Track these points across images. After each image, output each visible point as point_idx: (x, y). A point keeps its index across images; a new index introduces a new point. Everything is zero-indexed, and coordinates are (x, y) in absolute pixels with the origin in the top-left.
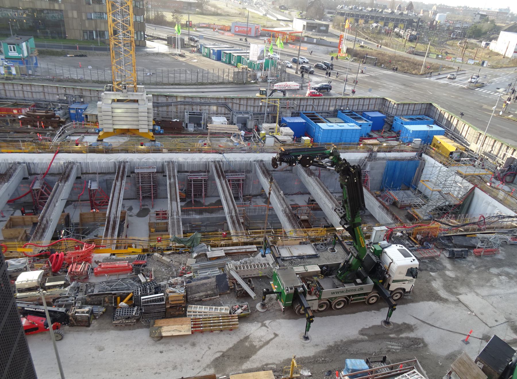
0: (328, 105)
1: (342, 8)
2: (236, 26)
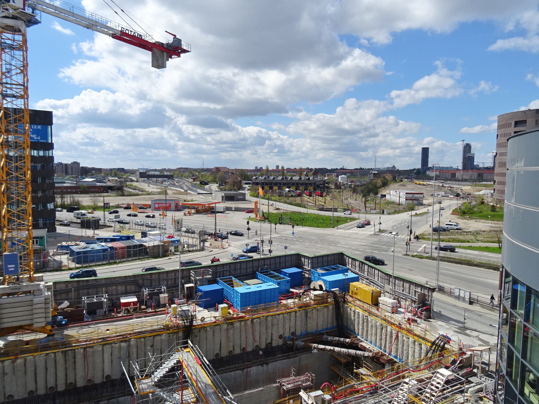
0: (245, 267)
1: (256, 178)
2: (155, 204)
